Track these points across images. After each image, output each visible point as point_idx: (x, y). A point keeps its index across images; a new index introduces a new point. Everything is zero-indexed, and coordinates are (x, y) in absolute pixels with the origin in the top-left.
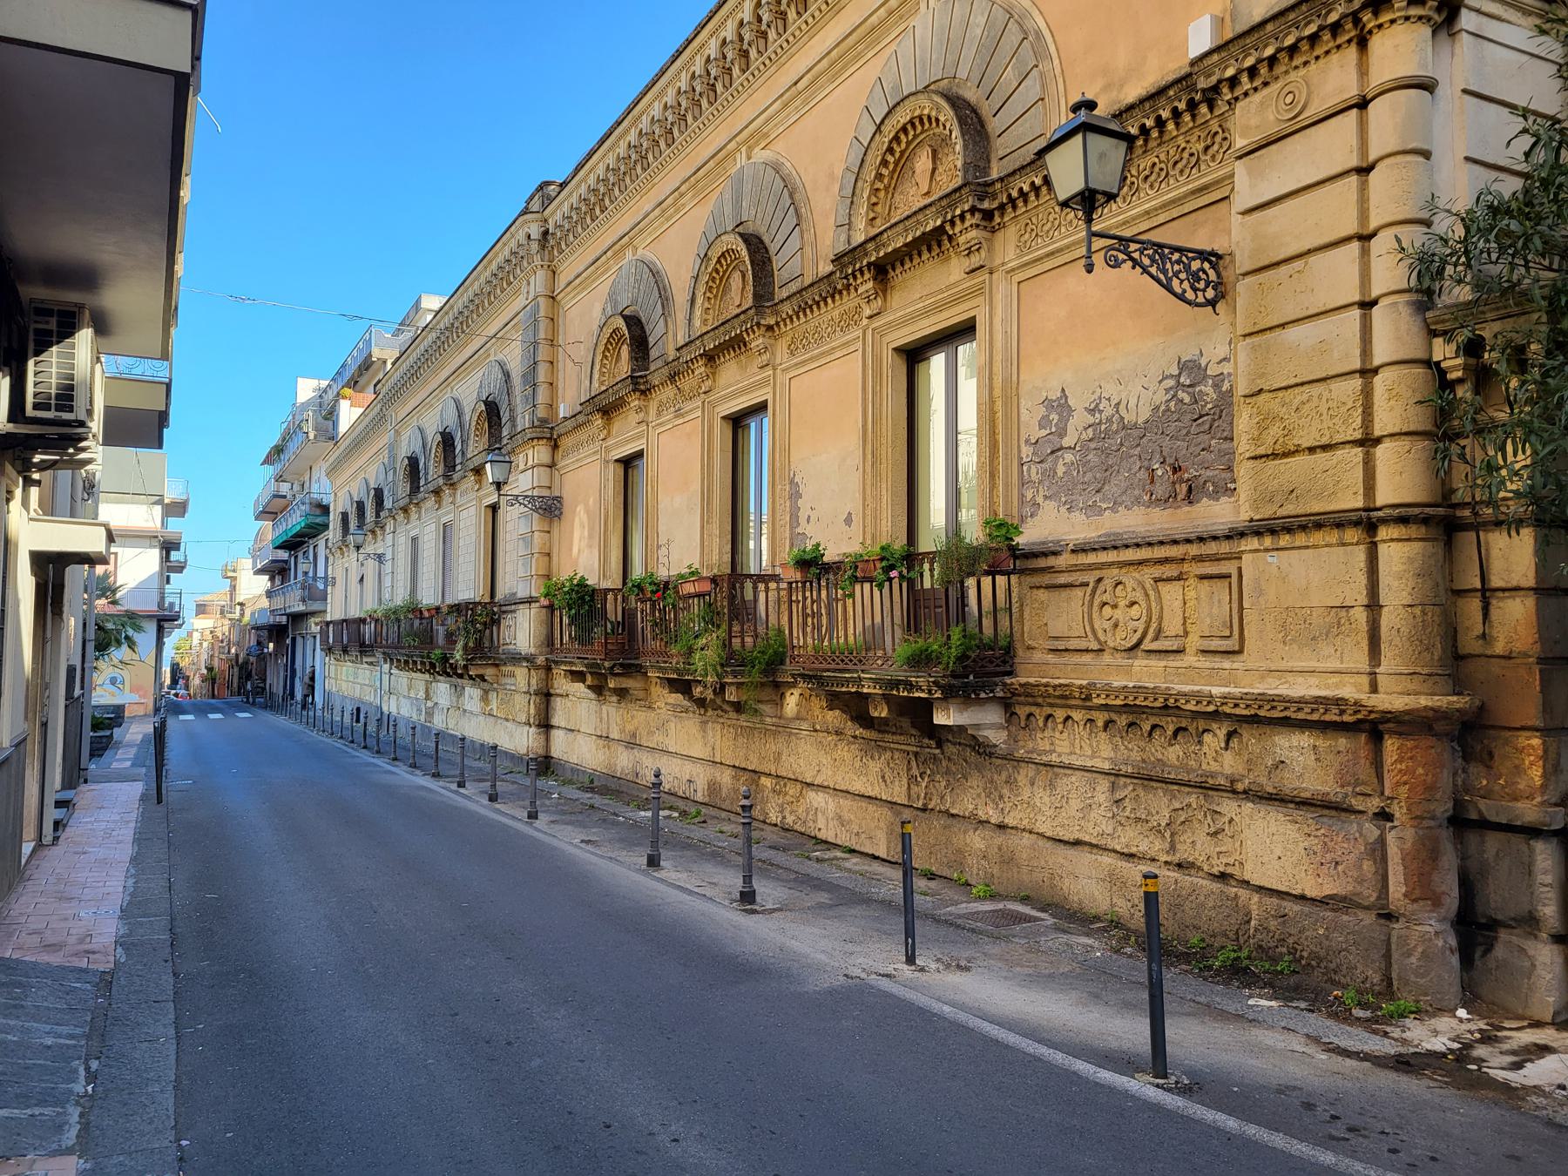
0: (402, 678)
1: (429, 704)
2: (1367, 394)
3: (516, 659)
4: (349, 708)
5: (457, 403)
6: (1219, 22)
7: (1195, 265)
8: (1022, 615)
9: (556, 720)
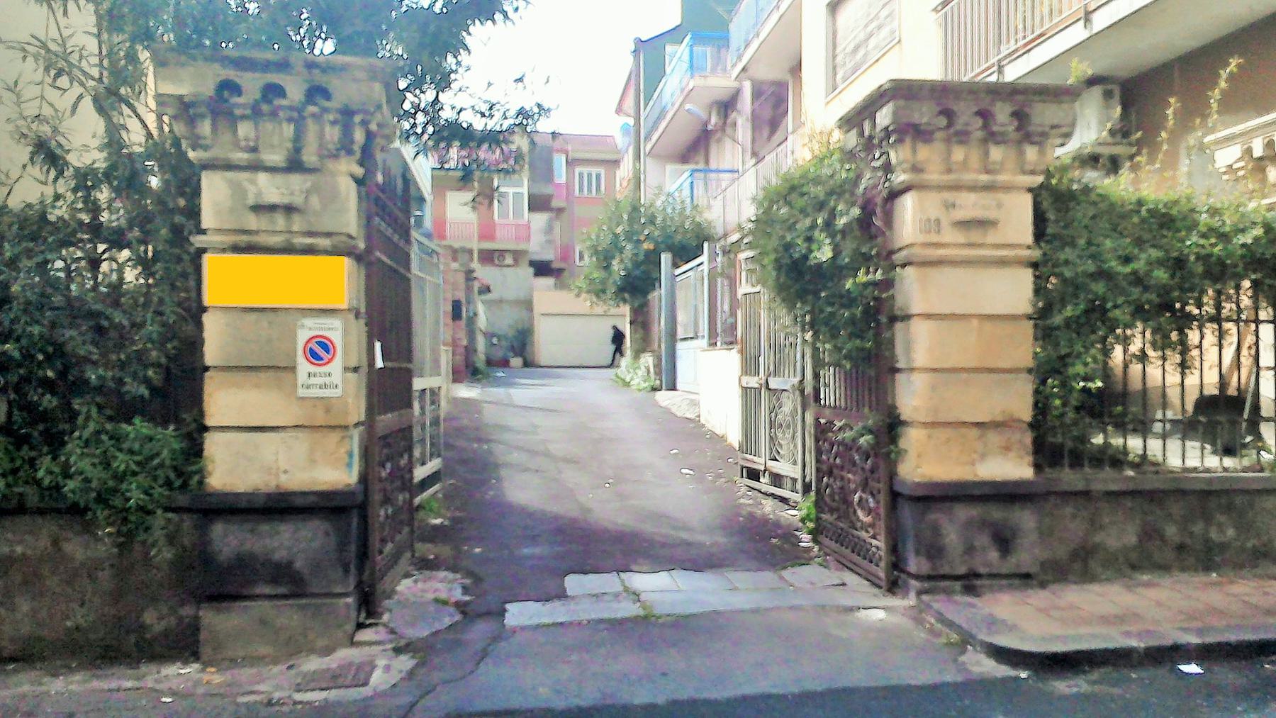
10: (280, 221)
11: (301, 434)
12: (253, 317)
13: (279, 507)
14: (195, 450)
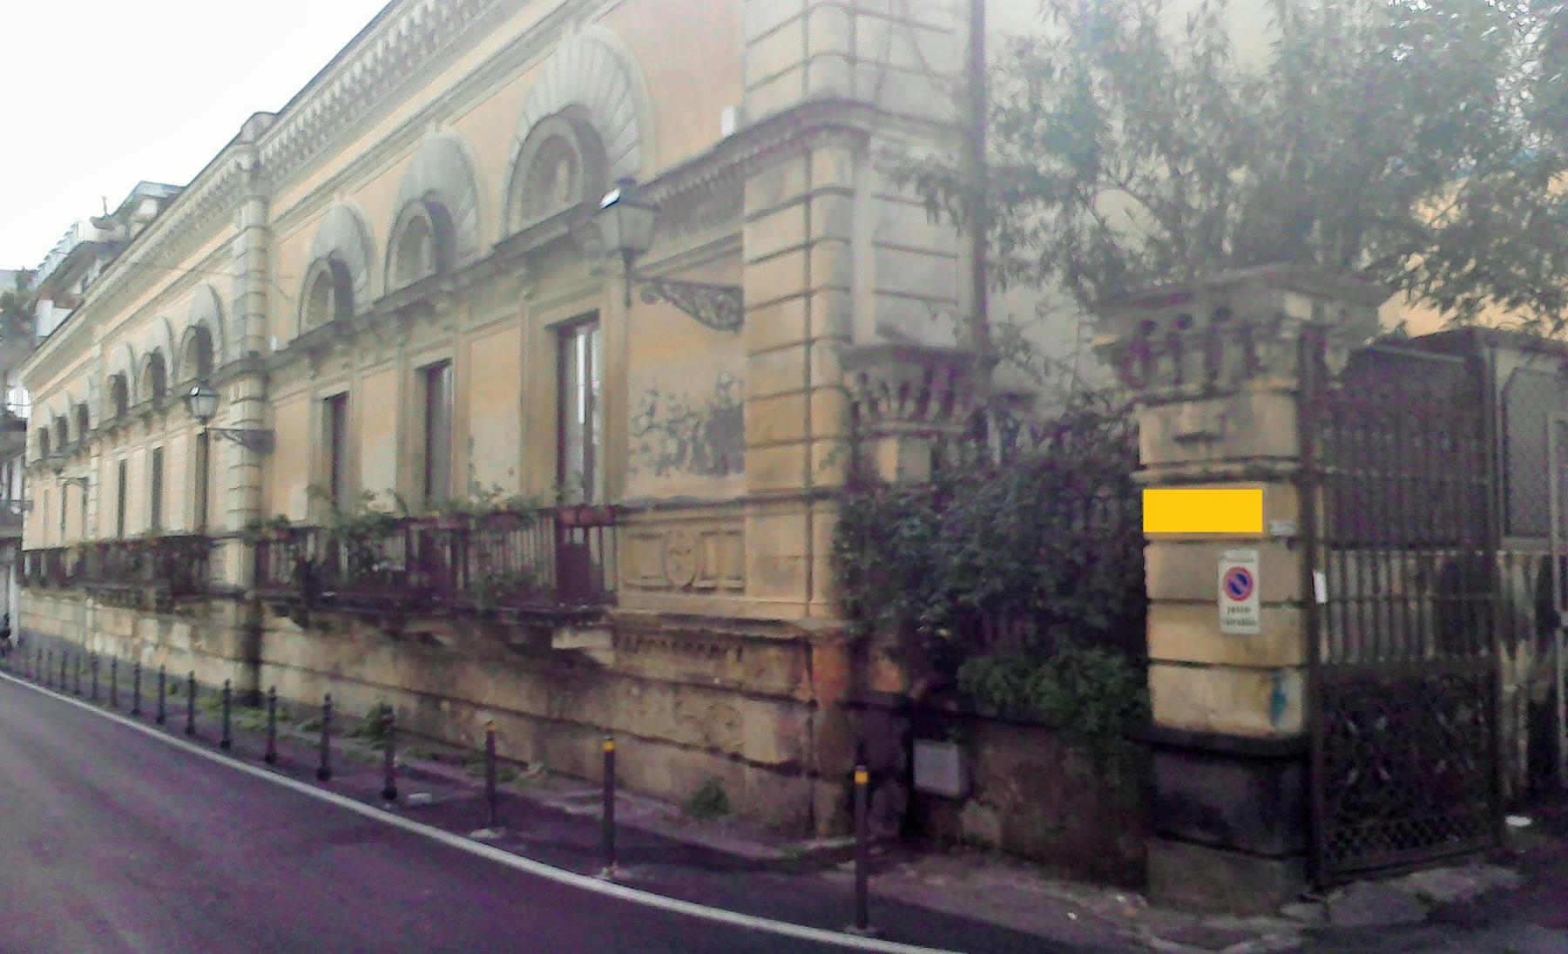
0: (106, 615)
1: (137, 641)
2: (808, 404)
3: (224, 594)
4: (57, 654)
5: (168, 323)
6: (741, 113)
7: (720, 298)
8: (615, 555)
9: (268, 654)
10: (1202, 451)
11: (1226, 673)
12: (1183, 548)
13: (1204, 748)
14: (1142, 682)
